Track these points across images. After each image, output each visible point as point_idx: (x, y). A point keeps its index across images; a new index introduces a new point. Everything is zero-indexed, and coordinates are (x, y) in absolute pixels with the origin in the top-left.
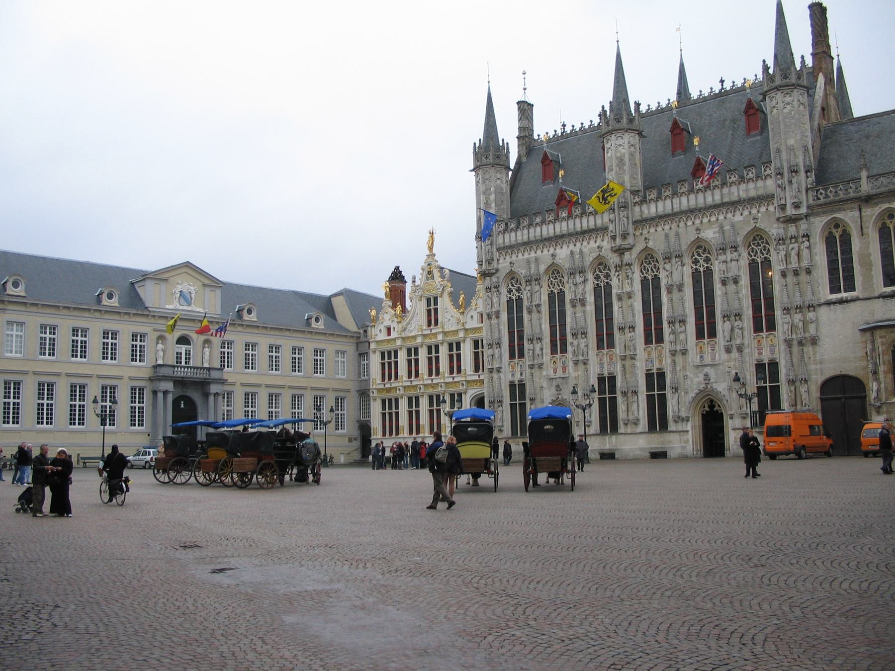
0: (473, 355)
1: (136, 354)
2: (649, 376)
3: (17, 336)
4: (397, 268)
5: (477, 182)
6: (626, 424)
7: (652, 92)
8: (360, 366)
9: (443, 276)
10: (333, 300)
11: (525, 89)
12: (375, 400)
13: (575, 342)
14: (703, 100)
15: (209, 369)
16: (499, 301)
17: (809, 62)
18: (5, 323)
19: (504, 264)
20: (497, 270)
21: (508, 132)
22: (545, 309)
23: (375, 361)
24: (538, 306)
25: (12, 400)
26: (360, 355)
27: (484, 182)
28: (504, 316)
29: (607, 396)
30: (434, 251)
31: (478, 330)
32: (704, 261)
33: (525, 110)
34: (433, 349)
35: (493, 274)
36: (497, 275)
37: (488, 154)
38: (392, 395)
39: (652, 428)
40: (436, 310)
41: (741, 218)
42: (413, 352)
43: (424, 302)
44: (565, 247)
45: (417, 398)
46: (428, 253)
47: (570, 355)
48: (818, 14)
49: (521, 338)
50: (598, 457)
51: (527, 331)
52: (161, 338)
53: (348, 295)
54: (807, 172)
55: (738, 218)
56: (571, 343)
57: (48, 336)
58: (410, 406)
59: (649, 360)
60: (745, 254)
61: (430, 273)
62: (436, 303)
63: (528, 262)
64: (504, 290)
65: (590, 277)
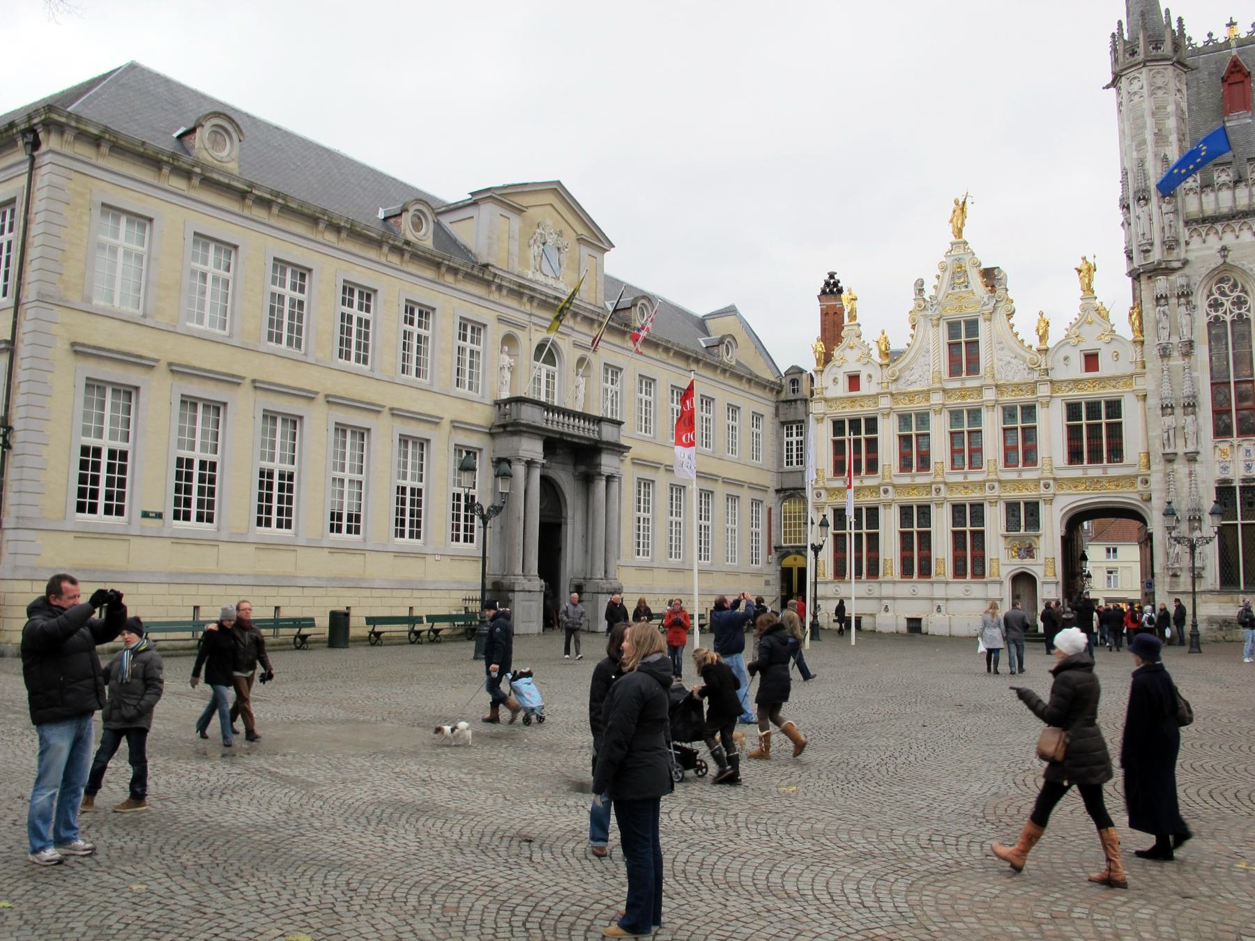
16: (1192, 322)
18: (190, 237)
19: (1203, 251)
20: (1186, 263)
23: (820, 440)
27: (1152, 94)
29: (915, 528)
30: (965, 236)
35: (1174, 270)
36: (1187, 270)
43: (943, 330)
46: (953, 239)
57: (288, 292)
64: (1200, 300)
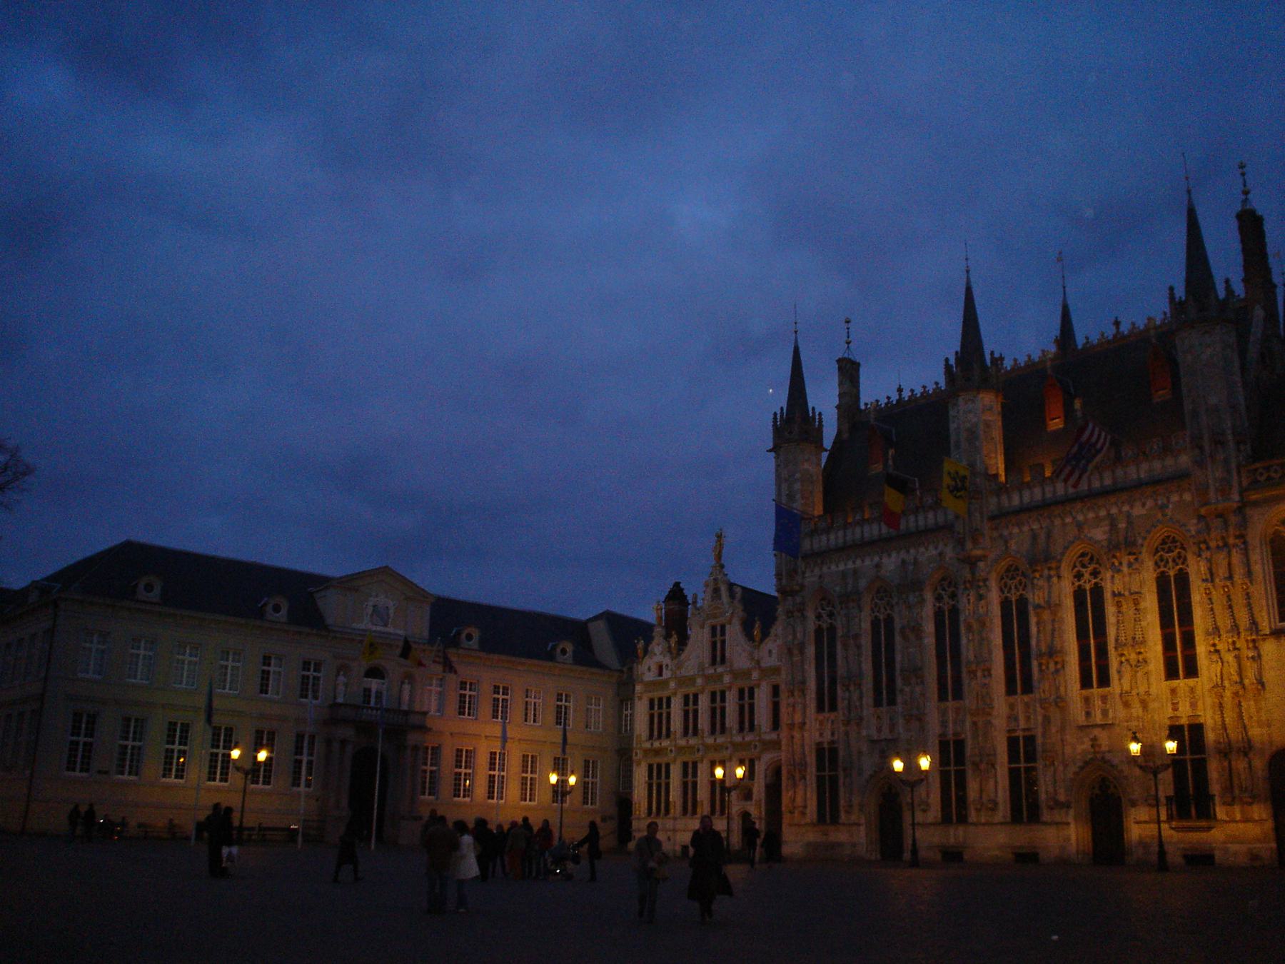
0: (771, 706)
1: (307, 687)
2: (1012, 743)
3: (190, 662)
4: (677, 585)
5: (778, 466)
6: (978, 810)
7: (1020, 338)
8: (620, 717)
9: (732, 595)
10: (592, 626)
11: (848, 343)
12: (639, 764)
13: (907, 689)
14: (1088, 347)
15: (406, 713)
17: (1239, 289)
19: (810, 578)
21: (824, 399)
22: (866, 642)
23: (641, 712)
24: (857, 636)
25: (82, 739)
26: (622, 701)
28: (811, 650)
31: (776, 671)
32: (1091, 574)
33: (849, 371)
34: (718, 698)
37: (794, 425)
38: (663, 760)
39: (1016, 817)
40: (723, 642)
41: (1143, 512)
42: (690, 701)
44: (894, 554)
45: (695, 764)
47: (899, 708)
48: (1250, 225)
49: (833, 681)
50: (939, 856)
51: (841, 671)
52: (343, 669)
53: (610, 618)
54: (1238, 443)
55: (1138, 511)
56: (902, 691)
58: (685, 774)
59: (1012, 718)
60: (1149, 564)
61: (716, 591)
62: (723, 633)
63: (844, 575)
64: (811, 615)
65: (929, 596)
